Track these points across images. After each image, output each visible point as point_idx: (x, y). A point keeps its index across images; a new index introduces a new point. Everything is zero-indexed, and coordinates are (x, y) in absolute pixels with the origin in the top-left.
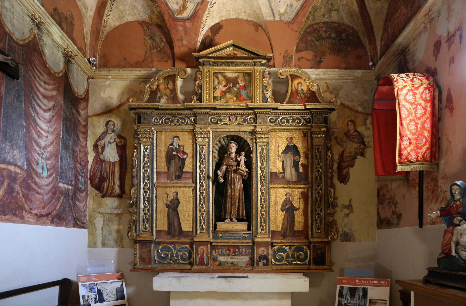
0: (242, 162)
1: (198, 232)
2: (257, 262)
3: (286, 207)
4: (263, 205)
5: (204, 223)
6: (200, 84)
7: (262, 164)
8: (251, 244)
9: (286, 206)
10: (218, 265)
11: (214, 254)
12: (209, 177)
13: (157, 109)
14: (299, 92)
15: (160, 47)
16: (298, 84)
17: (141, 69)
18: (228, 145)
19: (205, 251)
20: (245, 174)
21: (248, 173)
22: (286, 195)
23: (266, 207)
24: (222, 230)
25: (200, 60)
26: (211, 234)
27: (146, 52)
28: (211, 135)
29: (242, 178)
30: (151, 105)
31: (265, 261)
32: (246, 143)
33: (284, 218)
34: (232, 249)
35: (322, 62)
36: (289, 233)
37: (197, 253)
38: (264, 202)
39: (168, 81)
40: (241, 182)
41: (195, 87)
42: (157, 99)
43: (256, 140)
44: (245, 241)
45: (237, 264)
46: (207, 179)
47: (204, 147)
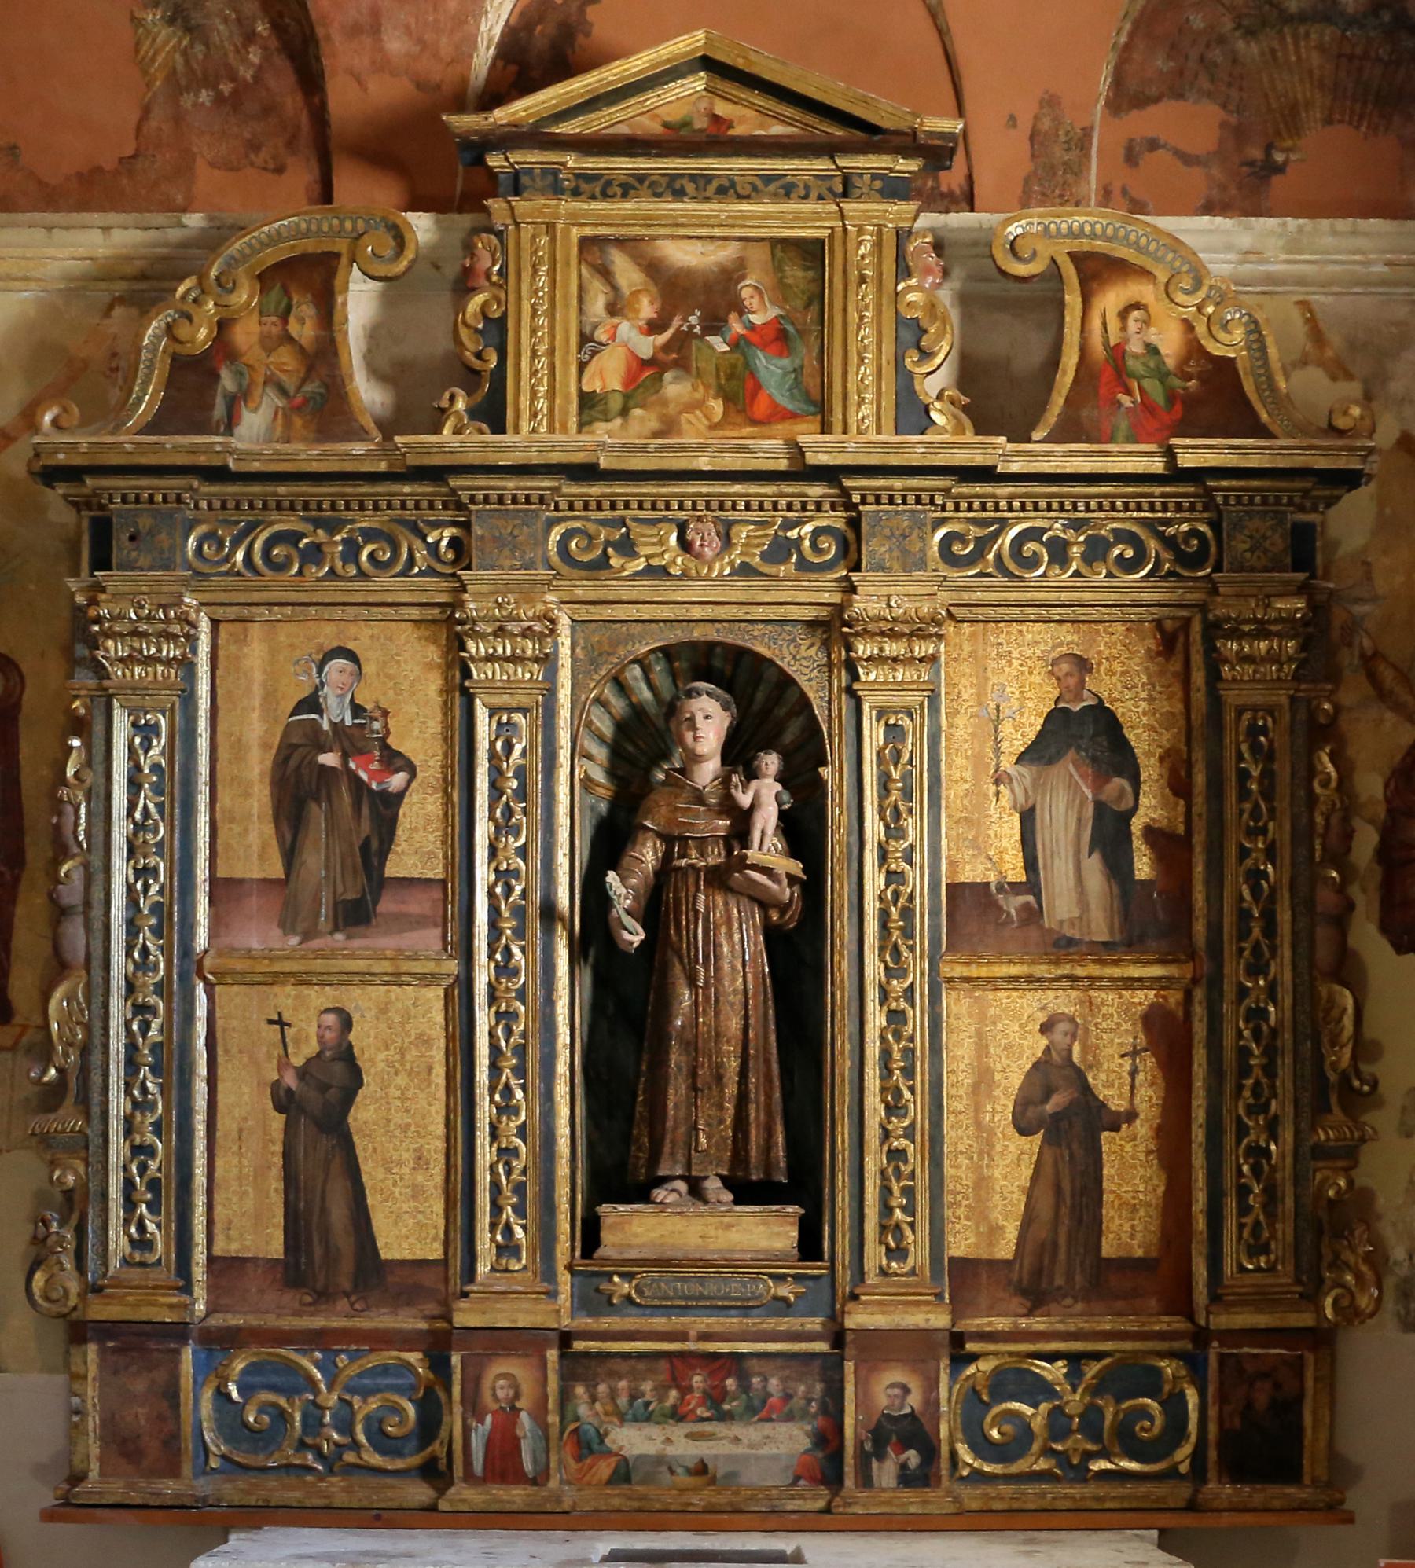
0: (767, 818)
1: (483, 1268)
2: (863, 1461)
3: (1049, 1108)
5: (520, 1211)
6: (495, 312)
7: (894, 830)
8: (822, 1346)
9: (1046, 1098)
10: (610, 1482)
11: (583, 1410)
12: (549, 912)
13: (218, 474)
14: (1130, 362)
15: (233, 77)
16: (1123, 314)
17: (112, 218)
18: (672, 709)
19: (527, 1388)
21: (804, 886)
22: (1046, 1028)
23: (916, 1108)
25: (494, 161)
26: (564, 1279)
27: (146, 111)
29: (766, 918)
30: (176, 448)
31: (912, 1457)
32: (791, 696)
33: (1034, 1180)
34: (697, 1380)
35: (1280, 169)
36: (1069, 1277)
37: (473, 1405)
38: (909, 1072)
39: (286, 292)
41: (464, 333)
42: (219, 411)
43: (855, 677)
44: (785, 1324)
45: (731, 1476)
46: (536, 926)
47: (517, 717)
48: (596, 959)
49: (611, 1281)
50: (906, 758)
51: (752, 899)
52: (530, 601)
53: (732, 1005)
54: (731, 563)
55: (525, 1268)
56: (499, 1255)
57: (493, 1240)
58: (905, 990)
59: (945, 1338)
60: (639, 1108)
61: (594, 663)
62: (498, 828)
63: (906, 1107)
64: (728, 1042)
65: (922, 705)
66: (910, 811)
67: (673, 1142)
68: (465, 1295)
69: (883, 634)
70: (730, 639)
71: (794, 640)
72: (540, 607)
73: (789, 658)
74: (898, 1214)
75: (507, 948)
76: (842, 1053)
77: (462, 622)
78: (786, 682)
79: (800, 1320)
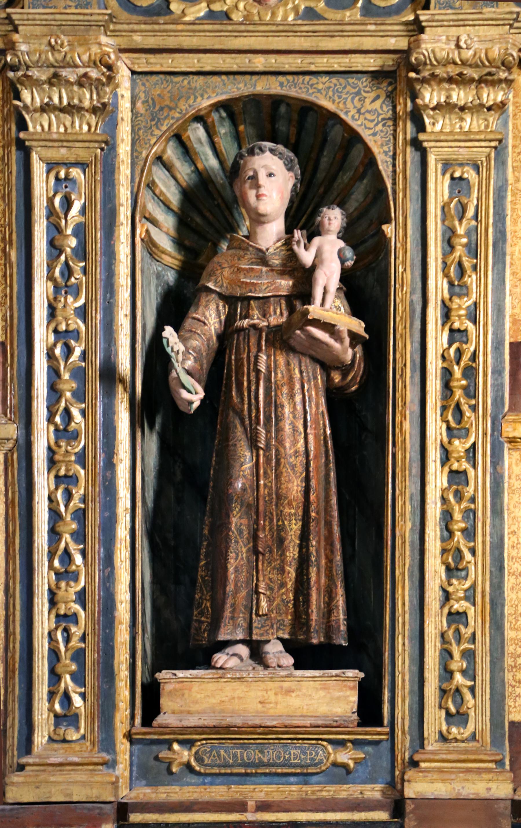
0: (329, 277)
1: (40, 739)
4: (459, 554)
5: (79, 678)
7: (458, 288)
8: (382, 816)
12: (109, 375)
18: (234, 171)
20: (347, 353)
21: (366, 345)
23: (477, 569)
24: (192, 721)
26: (123, 747)
28: (125, 90)
29: (329, 380)
32: (356, 155)
38: (470, 533)
40: (317, 406)
43: (421, 127)
46: (95, 386)
47: (76, 173)
48: (164, 426)
49: (170, 748)
50: (470, 212)
51: (315, 360)
52: (85, 43)
53: (293, 467)
54: (296, 9)
55: (84, 737)
56: (57, 725)
57: (51, 709)
58: (467, 451)
59: (506, 809)
60: (201, 572)
61: (155, 118)
62: (57, 288)
63: (466, 569)
64: (290, 504)
65: (488, 157)
66: (475, 268)
67: (233, 605)
68: (21, 768)
69: (450, 80)
70: (293, 93)
71: (358, 93)
72: (95, 49)
73: (353, 112)
74: (458, 678)
75: (67, 412)
76: (403, 514)
77: (14, 68)
78: (354, 138)
79: (359, 787)
